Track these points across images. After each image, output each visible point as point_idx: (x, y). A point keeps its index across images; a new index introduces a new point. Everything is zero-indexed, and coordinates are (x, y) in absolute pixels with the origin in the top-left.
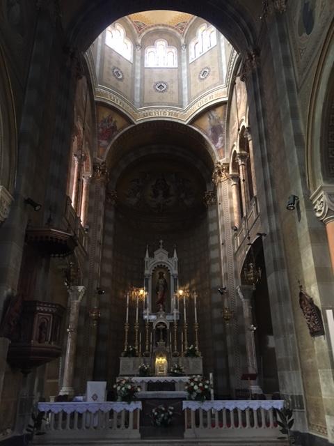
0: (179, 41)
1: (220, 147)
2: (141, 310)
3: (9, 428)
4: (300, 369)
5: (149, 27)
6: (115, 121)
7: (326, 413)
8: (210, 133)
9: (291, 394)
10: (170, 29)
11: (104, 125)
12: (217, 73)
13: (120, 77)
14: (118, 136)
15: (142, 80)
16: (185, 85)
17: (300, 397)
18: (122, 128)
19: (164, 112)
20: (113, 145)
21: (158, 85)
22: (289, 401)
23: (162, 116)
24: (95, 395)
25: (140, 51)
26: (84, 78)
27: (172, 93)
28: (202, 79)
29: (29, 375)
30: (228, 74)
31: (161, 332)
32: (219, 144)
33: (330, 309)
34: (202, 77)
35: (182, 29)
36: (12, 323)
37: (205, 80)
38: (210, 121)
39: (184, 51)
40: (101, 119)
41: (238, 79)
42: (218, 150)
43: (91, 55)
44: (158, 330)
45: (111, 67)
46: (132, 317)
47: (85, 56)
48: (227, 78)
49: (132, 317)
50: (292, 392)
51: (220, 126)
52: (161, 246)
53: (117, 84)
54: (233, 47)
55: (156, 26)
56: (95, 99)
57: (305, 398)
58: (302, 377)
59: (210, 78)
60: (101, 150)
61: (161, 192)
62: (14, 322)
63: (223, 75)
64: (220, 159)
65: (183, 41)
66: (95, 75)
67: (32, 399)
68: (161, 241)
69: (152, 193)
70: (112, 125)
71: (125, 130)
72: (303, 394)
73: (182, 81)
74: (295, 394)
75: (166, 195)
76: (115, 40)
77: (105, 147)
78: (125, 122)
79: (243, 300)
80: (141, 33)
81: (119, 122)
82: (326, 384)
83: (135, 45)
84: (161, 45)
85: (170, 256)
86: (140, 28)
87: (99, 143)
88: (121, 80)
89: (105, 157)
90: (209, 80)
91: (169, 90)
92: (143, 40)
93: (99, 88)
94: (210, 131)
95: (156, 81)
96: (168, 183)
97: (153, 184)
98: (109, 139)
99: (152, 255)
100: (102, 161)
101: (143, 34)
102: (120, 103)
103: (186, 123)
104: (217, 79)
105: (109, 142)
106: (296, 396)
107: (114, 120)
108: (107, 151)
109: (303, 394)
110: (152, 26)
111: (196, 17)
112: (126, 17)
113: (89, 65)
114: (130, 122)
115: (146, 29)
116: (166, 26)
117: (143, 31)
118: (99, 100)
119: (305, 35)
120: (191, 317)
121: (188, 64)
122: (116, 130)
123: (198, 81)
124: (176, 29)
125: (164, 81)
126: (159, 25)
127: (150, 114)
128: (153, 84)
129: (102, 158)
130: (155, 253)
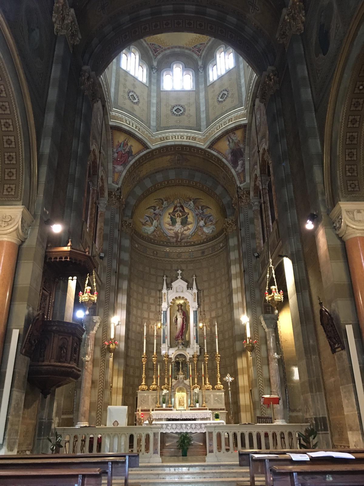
0: (198, 64)
1: (240, 171)
2: (159, 345)
3: (28, 450)
4: (323, 390)
5: (165, 50)
6: (131, 146)
7: (348, 429)
8: (230, 157)
9: (315, 417)
10: (187, 51)
11: (120, 149)
12: (236, 95)
13: (135, 101)
14: (134, 161)
15: (159, 103)
16: (203, 108)
17: (324, 419)
18: (138, 153)
19: (182, 136)
20: (128, 171)
21: (175, 108)
22: (313, 423)
23: (79, 454)
24: (116, 421)
25: (156, 74)
26: (100, 102)
27: (189, 116)
28: (220, 102)
29: (49, 396)
30: (247, 96)
31: (180, 364)
32: (239, 168)
33: (350, 324)
34: (220, 100)
35: (199, 50)
36: (33, 342)
37: (224, 103)
38: (229, 145)
39: (201, 73)
40: (116, 143)
41: (257, 101)
42: (238, 174)
43: (105, 78)
44: (177, 363)
45: (127, 90)
46: (150, 352)
47: (100, 79)
48: (247, 100)
49: (150, 352)
50: (316, 415)
51: (240, 149)
52: (179, 277)
53: (133, 108)
54: (252, 68)
55: (172, 48)
56: (111, 123)
57: (329, 419)
58: (326, 398)
59: (229, 100)
60: (116, 175)
61: (179, 220)
62: (34, 340)
63: (242, 97)
64: (241, 183)
65: (200, 63)
66: (110, 97)
67: (50, 424)
68: (180, 272)
69: (169, 220)
70: (127, 150)
71: (142, 154)
72: (326, 416)
73: (199, 104)
74: (318, 417)
75: (184, 222)
76: (130, 63)
77: (120, 172)
78: (141, 147)
79: (267, 330)
80: (156, 56)
81: (135, 147)
82: (348, 400)
83: (151, 68)
84: (177, 69)
85: (189, 287)
86: (155, 51)
87: (114, 168)
88: (136, 103)
89: (120, 182)
90: (228, 103)
91: (186, 113)
92: (159, 63)
93: (114, 112)
94: (230, 155)
95: (173, 104)
96: (186, 210)
97: (171, 211)
98: (124, 164)
99: (169, 287)
100: (117, 186)
101: (159, 57)
102: (136, 128)
103: (204, 147)
104: (236, 102)
105: (125, 168)
106: (320, 418)
107: (129, 144)
108: (122, 177)
109: (326, 416)
110: (169, 48)
111: (213, 39)
112: (142, 40)
113: (104, 88)
114: (146, 147)
115: (162, 51)
116: (183, 48)
117: (159, 53)
118: (114, 124)
119: (321, 55)
120: (212, 351)
121: (206, 87)
122: (132, 155)
123: (216, 104)
124: (193, 51)
125: (182, 104)
126: (176, 47)
127: (166, 138)
128: (170, 107)
129: (117, 184)
130: (173, 284)
